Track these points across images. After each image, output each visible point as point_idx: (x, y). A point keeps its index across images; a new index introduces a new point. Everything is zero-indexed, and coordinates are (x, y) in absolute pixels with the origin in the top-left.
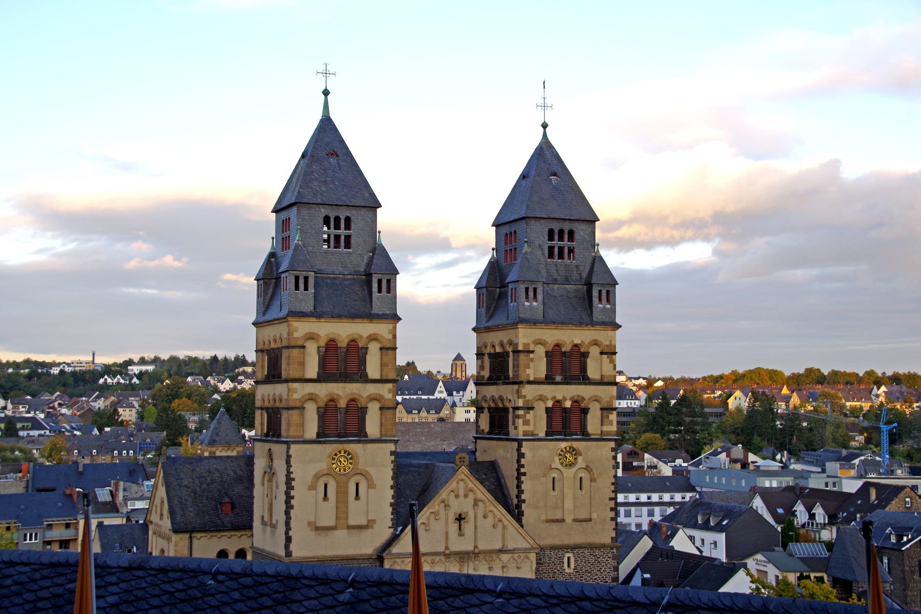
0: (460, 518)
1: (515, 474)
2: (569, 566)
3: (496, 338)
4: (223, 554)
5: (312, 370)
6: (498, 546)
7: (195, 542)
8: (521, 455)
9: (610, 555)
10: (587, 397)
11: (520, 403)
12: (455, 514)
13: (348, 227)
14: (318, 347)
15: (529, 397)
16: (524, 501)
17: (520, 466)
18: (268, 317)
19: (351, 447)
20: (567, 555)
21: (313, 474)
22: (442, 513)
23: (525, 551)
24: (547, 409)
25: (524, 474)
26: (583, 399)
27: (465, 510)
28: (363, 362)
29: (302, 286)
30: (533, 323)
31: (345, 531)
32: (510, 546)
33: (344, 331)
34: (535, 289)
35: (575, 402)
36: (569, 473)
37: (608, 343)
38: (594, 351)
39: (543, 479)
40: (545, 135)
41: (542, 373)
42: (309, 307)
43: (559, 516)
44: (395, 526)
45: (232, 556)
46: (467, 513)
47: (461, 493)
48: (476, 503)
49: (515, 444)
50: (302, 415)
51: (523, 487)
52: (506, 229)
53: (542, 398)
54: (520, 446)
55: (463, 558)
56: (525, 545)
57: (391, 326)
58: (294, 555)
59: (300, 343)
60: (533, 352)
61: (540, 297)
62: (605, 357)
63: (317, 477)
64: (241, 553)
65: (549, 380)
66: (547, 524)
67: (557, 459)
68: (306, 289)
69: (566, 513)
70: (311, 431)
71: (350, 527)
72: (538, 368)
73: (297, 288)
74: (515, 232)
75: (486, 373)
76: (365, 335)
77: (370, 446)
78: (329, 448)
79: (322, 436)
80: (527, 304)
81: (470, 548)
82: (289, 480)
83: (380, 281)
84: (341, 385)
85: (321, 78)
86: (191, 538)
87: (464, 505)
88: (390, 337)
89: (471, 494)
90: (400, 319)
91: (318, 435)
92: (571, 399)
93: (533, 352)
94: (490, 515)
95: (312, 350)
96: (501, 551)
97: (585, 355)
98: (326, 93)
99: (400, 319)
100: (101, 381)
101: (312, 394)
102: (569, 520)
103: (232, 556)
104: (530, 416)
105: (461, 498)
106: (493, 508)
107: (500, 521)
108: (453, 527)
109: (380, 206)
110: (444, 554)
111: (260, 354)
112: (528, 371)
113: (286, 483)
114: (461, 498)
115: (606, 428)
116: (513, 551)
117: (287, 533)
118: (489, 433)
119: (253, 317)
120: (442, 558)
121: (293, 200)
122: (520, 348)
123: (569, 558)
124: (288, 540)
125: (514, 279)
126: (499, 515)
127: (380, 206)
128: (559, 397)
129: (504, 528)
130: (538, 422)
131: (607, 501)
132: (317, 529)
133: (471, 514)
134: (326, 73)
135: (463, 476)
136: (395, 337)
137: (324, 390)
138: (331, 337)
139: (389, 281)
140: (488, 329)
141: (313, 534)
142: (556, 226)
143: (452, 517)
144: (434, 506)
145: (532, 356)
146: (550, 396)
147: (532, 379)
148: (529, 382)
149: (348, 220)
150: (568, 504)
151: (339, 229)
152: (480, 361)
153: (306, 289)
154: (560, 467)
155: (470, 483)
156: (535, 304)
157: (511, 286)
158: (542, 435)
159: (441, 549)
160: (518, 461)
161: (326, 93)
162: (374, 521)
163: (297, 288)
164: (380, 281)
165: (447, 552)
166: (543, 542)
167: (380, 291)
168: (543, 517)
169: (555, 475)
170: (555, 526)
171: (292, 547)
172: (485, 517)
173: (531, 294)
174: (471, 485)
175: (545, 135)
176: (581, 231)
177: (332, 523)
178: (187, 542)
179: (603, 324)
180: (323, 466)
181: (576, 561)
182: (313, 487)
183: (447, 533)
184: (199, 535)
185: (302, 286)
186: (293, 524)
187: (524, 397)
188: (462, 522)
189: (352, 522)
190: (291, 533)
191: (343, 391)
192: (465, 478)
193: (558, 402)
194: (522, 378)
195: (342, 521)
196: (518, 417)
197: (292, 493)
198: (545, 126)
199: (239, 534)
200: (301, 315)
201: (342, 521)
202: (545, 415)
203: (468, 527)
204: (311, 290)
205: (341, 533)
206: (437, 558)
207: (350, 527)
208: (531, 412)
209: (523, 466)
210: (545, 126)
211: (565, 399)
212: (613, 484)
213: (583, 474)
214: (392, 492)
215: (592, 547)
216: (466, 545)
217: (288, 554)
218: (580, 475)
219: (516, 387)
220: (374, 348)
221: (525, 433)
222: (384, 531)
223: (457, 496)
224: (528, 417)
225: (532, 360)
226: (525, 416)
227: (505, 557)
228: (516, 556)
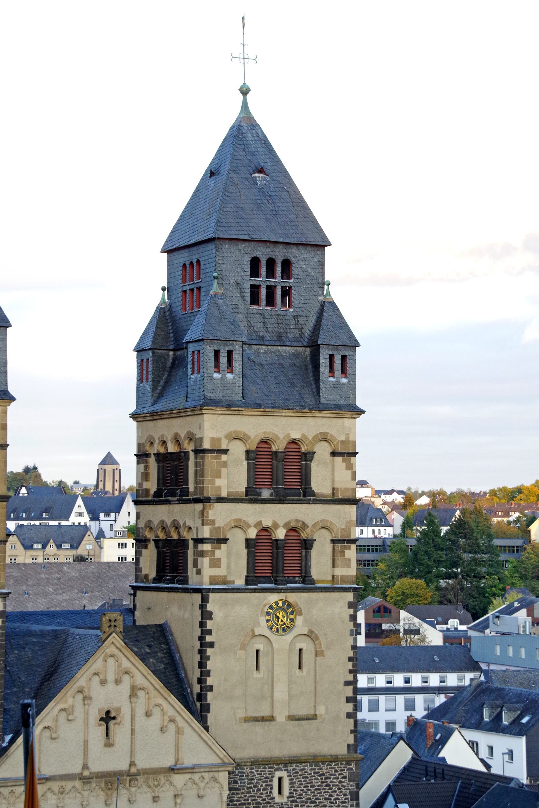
2: (280, 792)
3: (168, 430)
8: (206, 615)
9: (346, 773)
10: (310, 523)
11: (206, 532)
12: (100, 711)
16: (211, 688)
17: (205, 632)
20: (278, 774)
23: (211, 768)
25: (212, 645)
26: (304, 525)
32: (188, 761)
34: (230, 354)
35: (292, 529)
37: (343, 438)
38: (322, 451)
39: (241, 653)
40: (245, 106)
43: (265, 712)
46: (118, 710)
47: (111, 677)
49: (198, 597)
51: (210, 665)
53: (239, 525)
54: (205, 600)
55: (112, 784)
56: (212, 759)
61: (237, 365)
62: (339, 459)
65: (251, 496)
66: (246, 725)
67: (262, 620)
69: (277, 706)
72: (231, 475)
75: (152, 486)
80: (216, 376)
81: (124, 766)
89: (126, 678)
90: (13, 399)
92: (285, 525)
93: (226, 452)
94: (157, 712)
99: (13, 399)
102: (281, 718)
104: (221, 553)
106: (161, 701)
110: (82, 778)
112: (218, 482)
114: (111, 685)
115: (339, 572)
118: (155, 580)
120: (78, 784)
122: (206, 445)
123: (280, 779)
126: (171, 712)
128: (267, 523)
129: (179, 731)
130: (230, 563)
131: (341, 686)
133: (126, 712)
135: (113, 650)
140: (155, 416)
142: (263, 254)
143: (95, 715)
145: (224, 457)
146: (252, 521)
147: (224, 494)
148: (220, 500)
150: (281, 692)
151: (273, 277)
152: (142, 466)
154: (268, 633)
156: (229, 376)
158: (240, 582)
159: (76, 769)
160: (202, 624)
165: (86, 773)
168: (241, 714)
169: (261, 647)
170: (258, 727)
172: (148, 714)
173: (223, 360)
174: (126, 664)
175: (245, 106)
179: (337, 407)
181: (292, 784)
183: (86, 742)
187: (213, 522)
188: (112, 723)
192: (117, 652)
194: (209, 493)
196: (202, 554)
198: (245, 91)
203: (121, 732)
206: (68, 785)
208: (223, 546)
209: (210, 632)
210: (245, 91)
211: (276, 525)
212: (350, 659)
213: (306, 645)
215: (317, 760)
216: (115, 761)
218: (298, 646)
219: (199, 507)
221: (213, 580)
223: (103, 682)
224: (218, 554)
225: (225, 464)
226: (213, 553)
227: (179, 779)
228: (196, 777)
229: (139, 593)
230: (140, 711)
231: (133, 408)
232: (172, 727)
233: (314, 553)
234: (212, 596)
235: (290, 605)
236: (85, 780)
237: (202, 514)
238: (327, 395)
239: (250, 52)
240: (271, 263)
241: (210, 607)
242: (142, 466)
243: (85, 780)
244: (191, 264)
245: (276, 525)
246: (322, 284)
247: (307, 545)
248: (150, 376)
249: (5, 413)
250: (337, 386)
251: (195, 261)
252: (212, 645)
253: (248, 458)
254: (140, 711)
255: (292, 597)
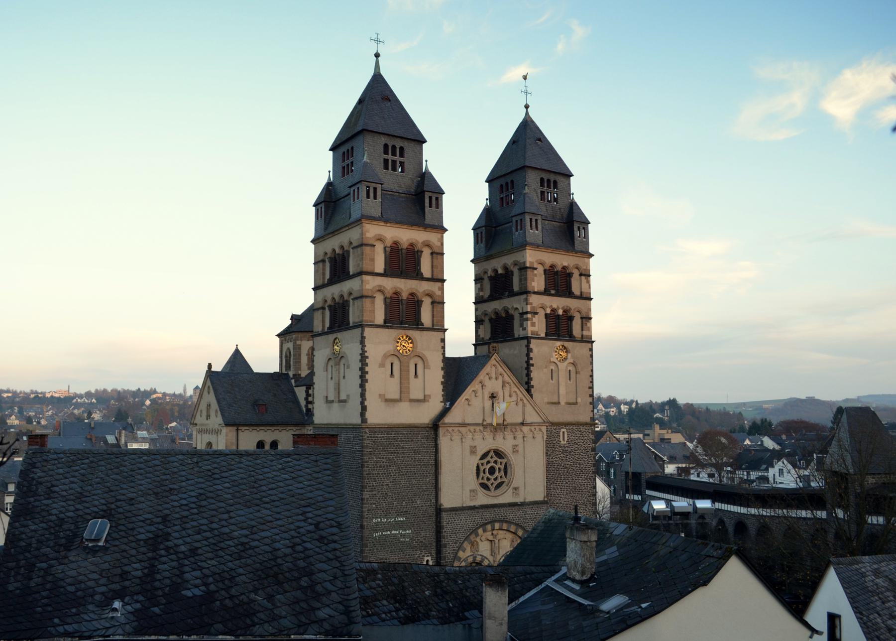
0: (493, 397)
1: (525, 365)
3: (498, 264)
4: (261, 444)
5: (380, 267)
6: (520, 421)
7: (240, 433)
8: (529, 350)
11: (529, 309)
13: (402, 155)
14: (385, 248)
15: (535, 305)
17: (529, 358)
18: (331, 229)
19: (411, 333)
20: (562, 430)
21: (383, 353)
22: (480, 393)
23: (539, 424)
24: (546, 315)
25: (533, 365)
27: (496, 390)
28: (417, 264)
29: (372, 195)
30: (536, 246)
31: (408, 403)
32: (528, 420)
33: (405, 235)
34: (536, 220)
36: (563, 366)
38: (576, 273)
39: (545, 370)
40: (527, 113)
41: (542, 288)
42: (376, 211)
43: (556, 400)
44: (445, 401)
45: (267, 447)
48: (504, 384)
49: (525, 342)
50: (373, 303)
51: (532, 375)
52: (497, 184)
53: (543, 307)
54: (529, 343)
56: (539, 420)
57: (439, 235)
58: (369, 422)
59: (371, 242)
60: (536, 269)
61: (540, 227)
62: (583, 278)
63: (385, 356)
64: (274, 444)
65: (546, 292)
68: (375, 198)
70: (380, 318)
71: (411, 401)
72: (537, 282)
73: (368, 197)
74: (512, 182)
75: (487, 293)
76: (421, 241)
77: (425, 333)
78: (393, 333)
79: (389, 323)
82: (363, 358)
83: (430, 198)
84: (403, 280)
85: (373, 43)
86: (237, 430)
87: (493, 385)
88: (439, 244)
90: (446, 230)
91: (385, 322)
93: (536, 269)
94: (514, 395)
95: (379, 249)
96: (522, 424)
97: (570, 275)
98: (377, 55)
99: (446, 230)
100: (74, 401)
101: (380, 286)
102: (563, 403)
103: (267, 447)
104: (535, 319)
105: (494, 380)
106: (516, 390)
107: (521, 400)
108: (488, 403)
109: (425, 141)
111: (321, 265)
112: (534, 284)
113: (361, 361)
114: (494, 380)
116: (530, 424)
117: (362, 403)
119: (312, 236)
120: (481, 428)
121: (360, 128)
122: (528, 265)
124: (364, 408)
125: (518, 212)
127: (425, 141)
128: (555, 306)
129: (524, 406)
130: (537, 325)
132: (387, 400)
133: (501, 394)
134: (377, 41)
136: (442, 244)
137: (391, 284)
138: (395, 239)
139: (437, 199)
140: (488, 258)
141: (383, 404)
142: (546, 176)
143: (487, 396)
144: (474, 386)
145: (535, 272)
146: (548, 304)
148: (535, 293)
149: (402, 149)
150: (562, 391)
151: (387, 154)
152: (479, 285)
153: (375, 198)
155: (500, 368)
157: (514, 219)
158: (543, 335)
159: (481, 422)
160: (528, 355)
161: (377, 55)
162: (429, 396)
163: (368, 197)
164: (430, 198)
166: (551, 419)
167: (430, 206)
168: (546, 400)
169: (553, 368)
170: (553, 407)
171: (368, 415)
174: (500, 370)
175: (527, 113)
176: (561, 180)
177: (397, 397)
178: (235, 433)
179: (582, 252)
180: (390, 348)
182: (382, 365)
184: (243, 428)
185: (372, 195)
186: (367, 395)
189: (412, 397)
190: (366, 403)
191: (405, 286)
193: (553, 310)
194: (529, 289)
195: (404, 395)
196: (527, 319)
197: (367, 369)
198: (527, 107)
199: (273, 428)
200: (372, 219)
201: (404, 395)
202: (544, 320)
204: (379, 199)
205: (404, 406)
207: (411, 401)
210: (527, 107)
211: (558, 308)
213: (571, 368)
214: (442, 373)
215: (579, 424)
217: (364, 420)
219: (524, 296)
220: (426, 253)
221: (533, 333)
222: (436, 405)
223: (490, 378)
224: (535, 320)
225: (536, 275)
228: (533, 428)
229: (588, 420)
230: (507, 394)
231: (472, 257)
232: (521, 404)
233: (574, 323)
234: (532, 341)
235: (565, 348)
236: (485, 426)
237: (526, 300)
238: (578, 246)
239: (529, 90)
240: (549, 181)
241: (531, 346)
242: (479, 285)
243: (485, 426)
244: (507, 184)
245: (558, 308)
246: (569, 194)
247: (571, 318)
248: (484, 239)
249: (442, 237)
250: (582, 242)
251: (509, 181)
252: (533, 365)
253: (545, 273)
254: (507, 394)
255: (566, 344)
